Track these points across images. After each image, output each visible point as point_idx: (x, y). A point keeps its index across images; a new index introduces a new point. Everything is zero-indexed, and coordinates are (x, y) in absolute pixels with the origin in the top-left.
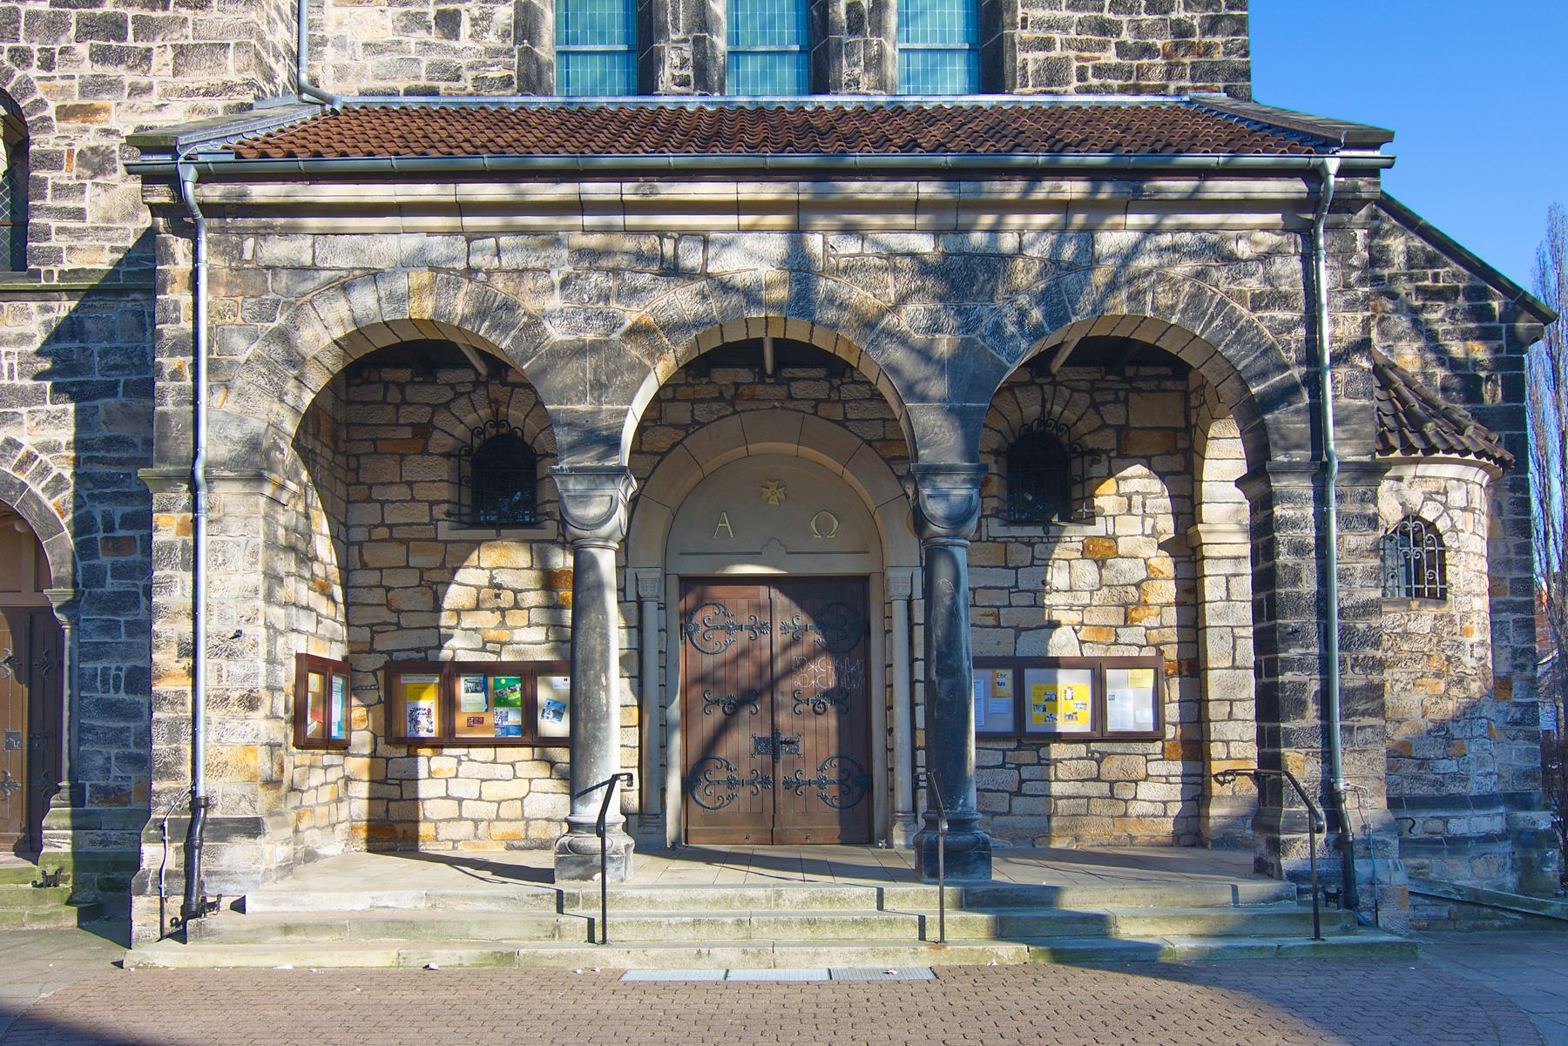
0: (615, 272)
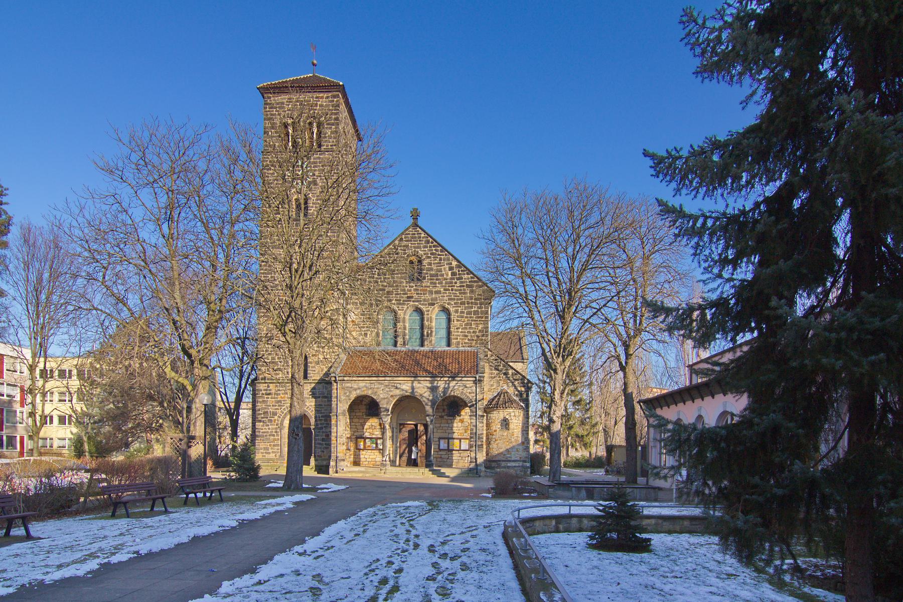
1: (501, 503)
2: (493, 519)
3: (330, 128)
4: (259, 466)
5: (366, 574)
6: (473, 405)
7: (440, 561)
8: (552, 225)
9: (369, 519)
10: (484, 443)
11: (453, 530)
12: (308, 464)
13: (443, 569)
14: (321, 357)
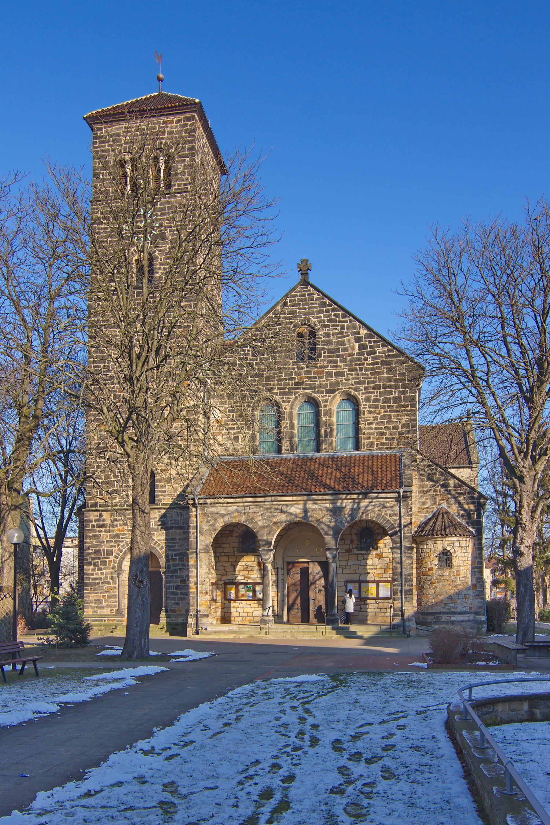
0: (271, 512)
1: (441, 677)
2: (431, 701)
4: (88, 627)
5: (240, 783)
6: (395, 533)
7: (350, 764)
8: (509, 268)
9: (245, 701)
10: (414, 588)
11: (369, 717)
12: (158, 623)
13: (356, 776)
14: (174, 472)
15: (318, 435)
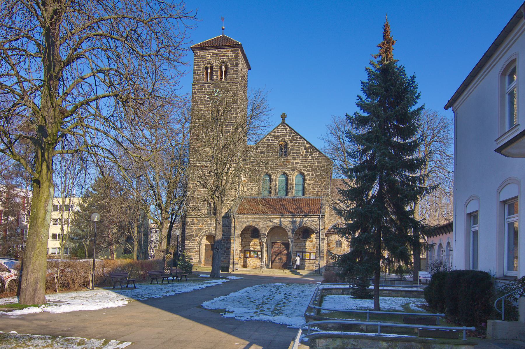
3: (233, 69)
6: (318, 232)
15: (287, 189)
